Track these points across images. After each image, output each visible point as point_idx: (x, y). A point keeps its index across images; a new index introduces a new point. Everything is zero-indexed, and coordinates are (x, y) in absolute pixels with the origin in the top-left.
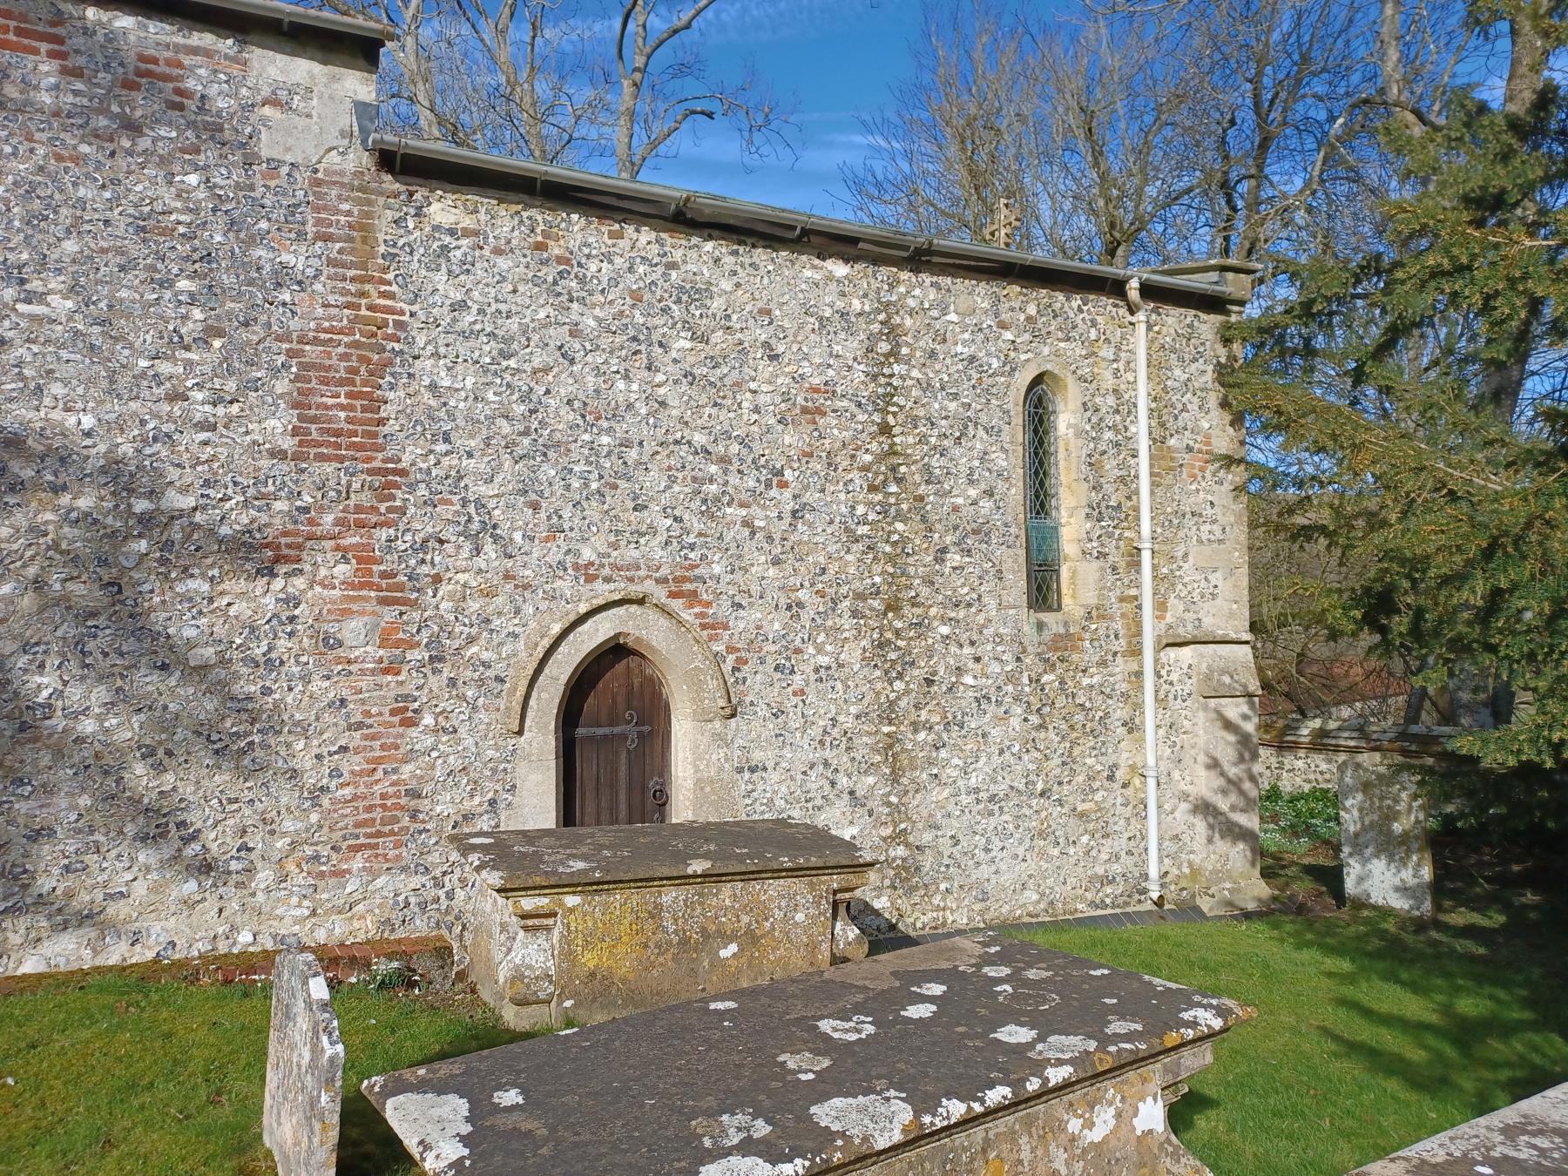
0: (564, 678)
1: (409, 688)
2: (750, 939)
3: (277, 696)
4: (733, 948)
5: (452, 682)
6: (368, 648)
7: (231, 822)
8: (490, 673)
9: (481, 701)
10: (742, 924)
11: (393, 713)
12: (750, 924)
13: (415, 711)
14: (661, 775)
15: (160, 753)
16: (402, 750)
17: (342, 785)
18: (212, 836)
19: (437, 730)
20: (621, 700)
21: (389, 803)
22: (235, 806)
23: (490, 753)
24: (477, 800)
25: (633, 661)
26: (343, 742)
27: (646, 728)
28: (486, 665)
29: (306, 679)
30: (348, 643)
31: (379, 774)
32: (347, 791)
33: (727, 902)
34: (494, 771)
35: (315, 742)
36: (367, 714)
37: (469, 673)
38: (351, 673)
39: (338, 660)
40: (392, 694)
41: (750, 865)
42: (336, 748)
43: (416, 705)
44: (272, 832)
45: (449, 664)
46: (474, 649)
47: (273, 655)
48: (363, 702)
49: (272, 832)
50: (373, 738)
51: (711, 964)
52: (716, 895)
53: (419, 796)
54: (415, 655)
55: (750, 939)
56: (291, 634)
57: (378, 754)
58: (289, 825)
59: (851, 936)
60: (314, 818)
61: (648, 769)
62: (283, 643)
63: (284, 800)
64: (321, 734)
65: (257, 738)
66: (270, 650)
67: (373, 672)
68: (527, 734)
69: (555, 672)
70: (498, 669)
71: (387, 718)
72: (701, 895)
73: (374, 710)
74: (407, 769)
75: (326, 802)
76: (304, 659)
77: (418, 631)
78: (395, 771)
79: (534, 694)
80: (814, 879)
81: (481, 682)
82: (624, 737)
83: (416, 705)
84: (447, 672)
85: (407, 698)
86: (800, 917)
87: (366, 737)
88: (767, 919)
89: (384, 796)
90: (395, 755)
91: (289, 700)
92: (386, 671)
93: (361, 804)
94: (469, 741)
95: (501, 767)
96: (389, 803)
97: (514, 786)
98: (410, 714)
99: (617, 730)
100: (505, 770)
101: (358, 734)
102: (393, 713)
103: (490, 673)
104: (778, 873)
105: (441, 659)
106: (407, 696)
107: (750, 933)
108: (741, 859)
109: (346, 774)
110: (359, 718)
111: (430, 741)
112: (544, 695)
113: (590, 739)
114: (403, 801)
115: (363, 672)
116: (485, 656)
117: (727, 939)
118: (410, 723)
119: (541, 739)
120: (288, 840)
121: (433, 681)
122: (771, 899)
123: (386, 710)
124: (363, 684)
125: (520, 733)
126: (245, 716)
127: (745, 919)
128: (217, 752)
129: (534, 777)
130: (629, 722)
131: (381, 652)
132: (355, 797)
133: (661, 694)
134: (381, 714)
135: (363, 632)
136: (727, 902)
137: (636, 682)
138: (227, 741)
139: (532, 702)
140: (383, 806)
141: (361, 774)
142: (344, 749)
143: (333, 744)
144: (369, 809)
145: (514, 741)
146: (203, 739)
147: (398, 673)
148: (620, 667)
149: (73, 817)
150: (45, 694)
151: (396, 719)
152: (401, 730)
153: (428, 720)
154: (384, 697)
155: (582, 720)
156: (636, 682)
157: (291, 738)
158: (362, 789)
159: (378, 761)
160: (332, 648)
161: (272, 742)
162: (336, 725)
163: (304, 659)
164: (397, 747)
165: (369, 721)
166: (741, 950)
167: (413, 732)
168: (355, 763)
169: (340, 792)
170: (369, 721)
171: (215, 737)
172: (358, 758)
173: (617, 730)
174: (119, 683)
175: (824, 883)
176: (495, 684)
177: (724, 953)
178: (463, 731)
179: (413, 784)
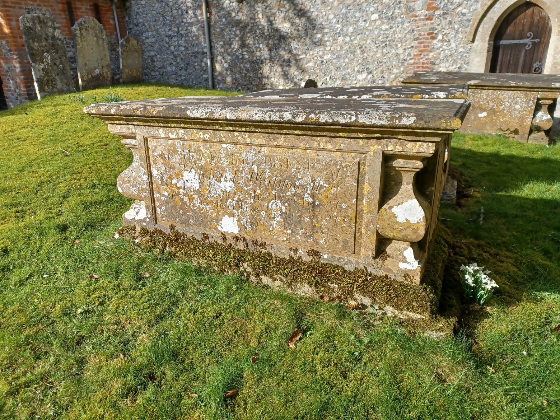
0: (496, 18)
1: (435, 25)
2: (492, 112)
3: (394, 29)
4: (485, 114)
5: (450, 22)
6: (423, 11)
7: (380, 69)
8: (465, 18)
9: (460, 29)
10: (490, 106)
11: (429, 34)
12: (493, 106)
13: (436, 34)
14: (540, 61)
15: (364, 47)
16: (430, 48)
17: (411, 59)
18: (375, 72)
19: (443, 41)
20: (526, 28)
21: (424, 66)
22: (381, 64)
23: (461, 50)
24: (454, 67)
25: (536, 9)
26: (412, 45)
27: (537, 40)
28: (464, 15)
29: (403, 23)
30: (416, 9)
31: (422, 56)
32: (412, 61)
33: (485, 97)
34: (462, 56)
35: (404, 44)
36: (420, 35)
37: (457, 18)
38: (416, 20)
39: (413, 16)
40: (429, 27)
41: (496, 83)
42: (409, 47)
43: (436, 31)
44: (390, 73)
45: (450, 16)
46: (460, 9)
47: (394, 15)
48: (419, 30)
49: (390, 73)
50: (421, 43)
51: (475, 118)
52: (480, 93)
53: (434, 64)
54: (438, 13)
55: (492, 112)
56: (399, 8)
57: (422, 49)
58: (395, 71)
59: (545, 118)
60: (402, 69)
61: (534, 58)
62: (397, 11)
63: (394, 63)
64: (406, 41)
65: (388, 43)
66: (393, 13)
67: (423, 20)
68: (476, 42)
69: (492, 16)
70: (469, 16)
71: (426, 36)
72: (473, 93)
73: (422, 33)
74: (431, 54)
75: (406, 64)
76: (402, 16)
77: (440, 3)
78: (427, 55)
79: (481, 26)
80: (528, 93)
81: (461, 22)
82: (525, 44)
83: (436, 31)
84: (449, 19)
85: (433, 29)
86: (518, 107)
87: (419, 43)
88: (501, 105)
89: (423, 63)
90: (427, 49)
91: (397, 30)
92: (428, 19)
93: (416, 66)
94: (453, 45)
95: (464, 55)
96: (424, 66)
97: (469, 62)
98: (434, 35)
99: (522, 41)
100: (466, 56)
101: (416, 42)
102: (429, 34)
103: (465, 18)
104: (510, 88)
105: (446, 14)
106: (433, 28)
107: (492, 109)
108: (493, 81)
109: (412, 55)
110: (417, 36)
111: (440, 44)
112: (486, 26)
113: (504, 45)
114: (429, 66)
115: (420, 20)
116: (464, 11)
117: (483, 110)
118: (433, 38)
119: (482, 44)
120: (394, 75)
121: (443, 22)
122: (504, 98)
123: (426, 33)
124: (420, 24)
125: (473, 41)
126: (385, 36)
127: (492, 104)
128: (377, 47)
129: (477, 59)
130: (528, 38)
131: (427, 12)
132: (414, 63)
133: (548, 24)
134: (424, 35)
135: (421, 5)
136: (485, 97)
137: (536, 19)
138: (380, 43)
139: (480, 29)
140: (423, 67)
141: (416, 55)
142: (412, 47)
143: (409, 45)
144: (418, 67)
145: (471, 45)
146: (374, 43)
147: (431, 20)
148: (529, 11)
149: (344, 65)
150: (339, 30)
151: (429, 37)
152: (430, 40)
153: (440, 37)
154: (426, 29)
155: (505, 37)
156: (536, 19)
157: (397, 43)
158: (417, 61)
159: (422, 51)
160: (411, 12)
161: (392, 44)
162: (410, 38)
163: (402, 16)
164: (428, 46)
165: (420, 37)
166: (488, 115)
167: (435, 41)
168: (415, 52)
169: (410, 61)
170: (420, 37)
171: (377, 42)
172: (416, 50)
173: (522, 41)
174: (355, 26)
175: (533, 94)
176: (466, 22)
177: (481, 115)
178: (452, 41)
179: (433, 60)
